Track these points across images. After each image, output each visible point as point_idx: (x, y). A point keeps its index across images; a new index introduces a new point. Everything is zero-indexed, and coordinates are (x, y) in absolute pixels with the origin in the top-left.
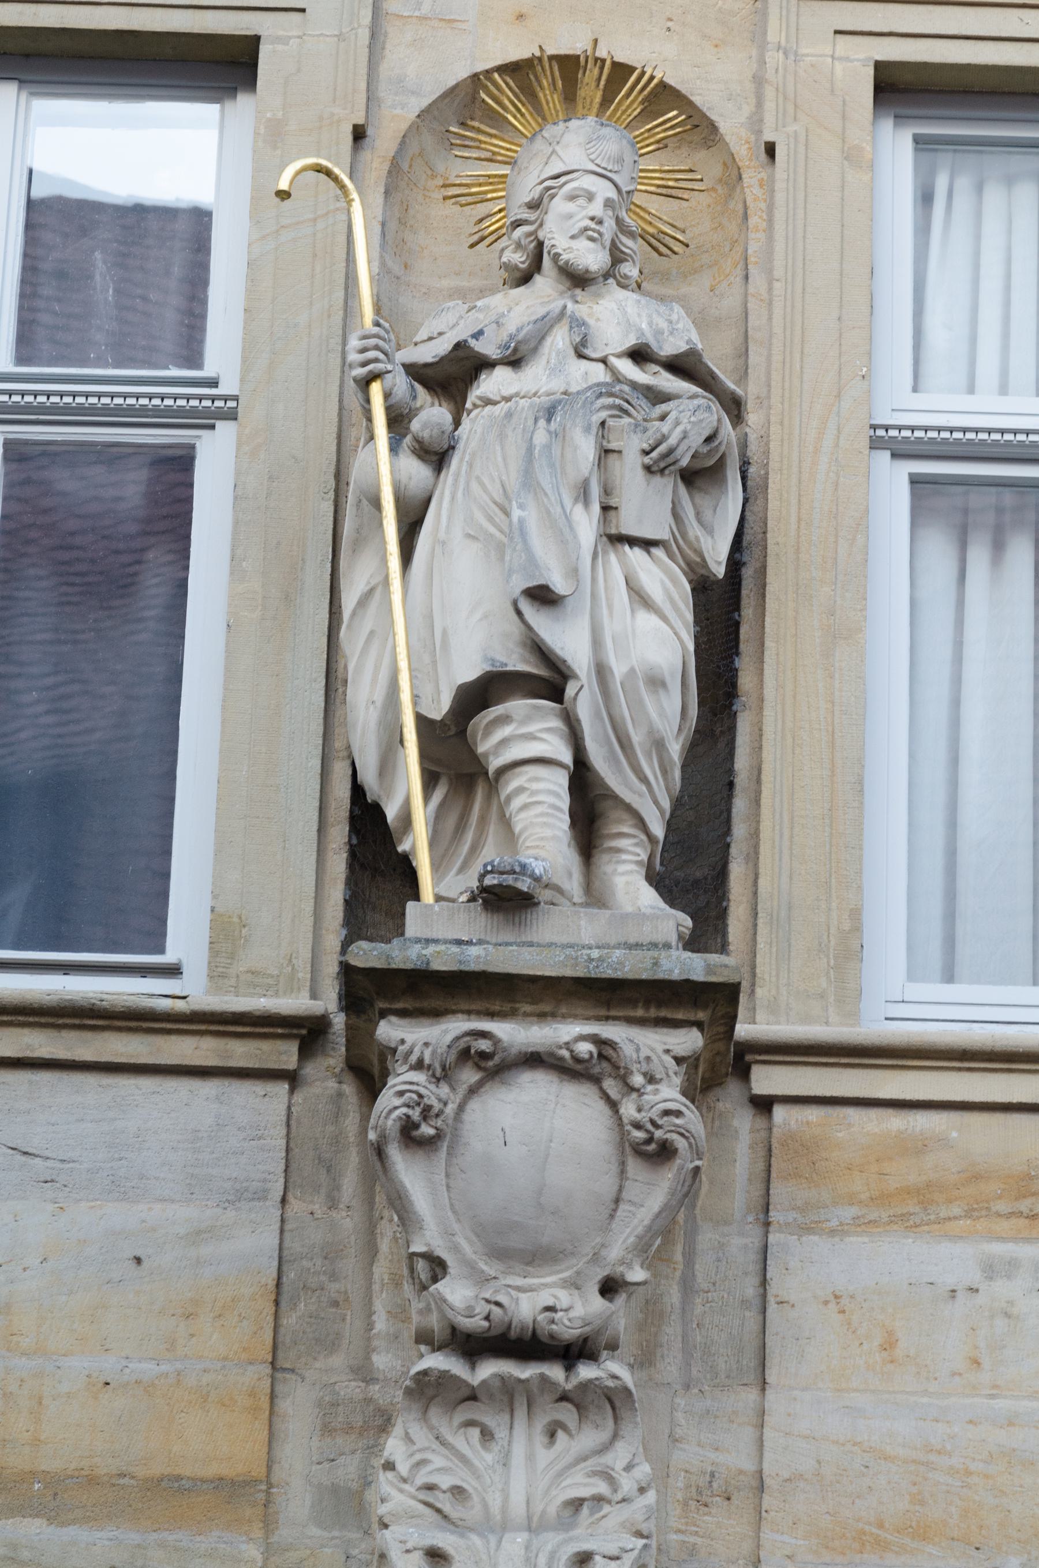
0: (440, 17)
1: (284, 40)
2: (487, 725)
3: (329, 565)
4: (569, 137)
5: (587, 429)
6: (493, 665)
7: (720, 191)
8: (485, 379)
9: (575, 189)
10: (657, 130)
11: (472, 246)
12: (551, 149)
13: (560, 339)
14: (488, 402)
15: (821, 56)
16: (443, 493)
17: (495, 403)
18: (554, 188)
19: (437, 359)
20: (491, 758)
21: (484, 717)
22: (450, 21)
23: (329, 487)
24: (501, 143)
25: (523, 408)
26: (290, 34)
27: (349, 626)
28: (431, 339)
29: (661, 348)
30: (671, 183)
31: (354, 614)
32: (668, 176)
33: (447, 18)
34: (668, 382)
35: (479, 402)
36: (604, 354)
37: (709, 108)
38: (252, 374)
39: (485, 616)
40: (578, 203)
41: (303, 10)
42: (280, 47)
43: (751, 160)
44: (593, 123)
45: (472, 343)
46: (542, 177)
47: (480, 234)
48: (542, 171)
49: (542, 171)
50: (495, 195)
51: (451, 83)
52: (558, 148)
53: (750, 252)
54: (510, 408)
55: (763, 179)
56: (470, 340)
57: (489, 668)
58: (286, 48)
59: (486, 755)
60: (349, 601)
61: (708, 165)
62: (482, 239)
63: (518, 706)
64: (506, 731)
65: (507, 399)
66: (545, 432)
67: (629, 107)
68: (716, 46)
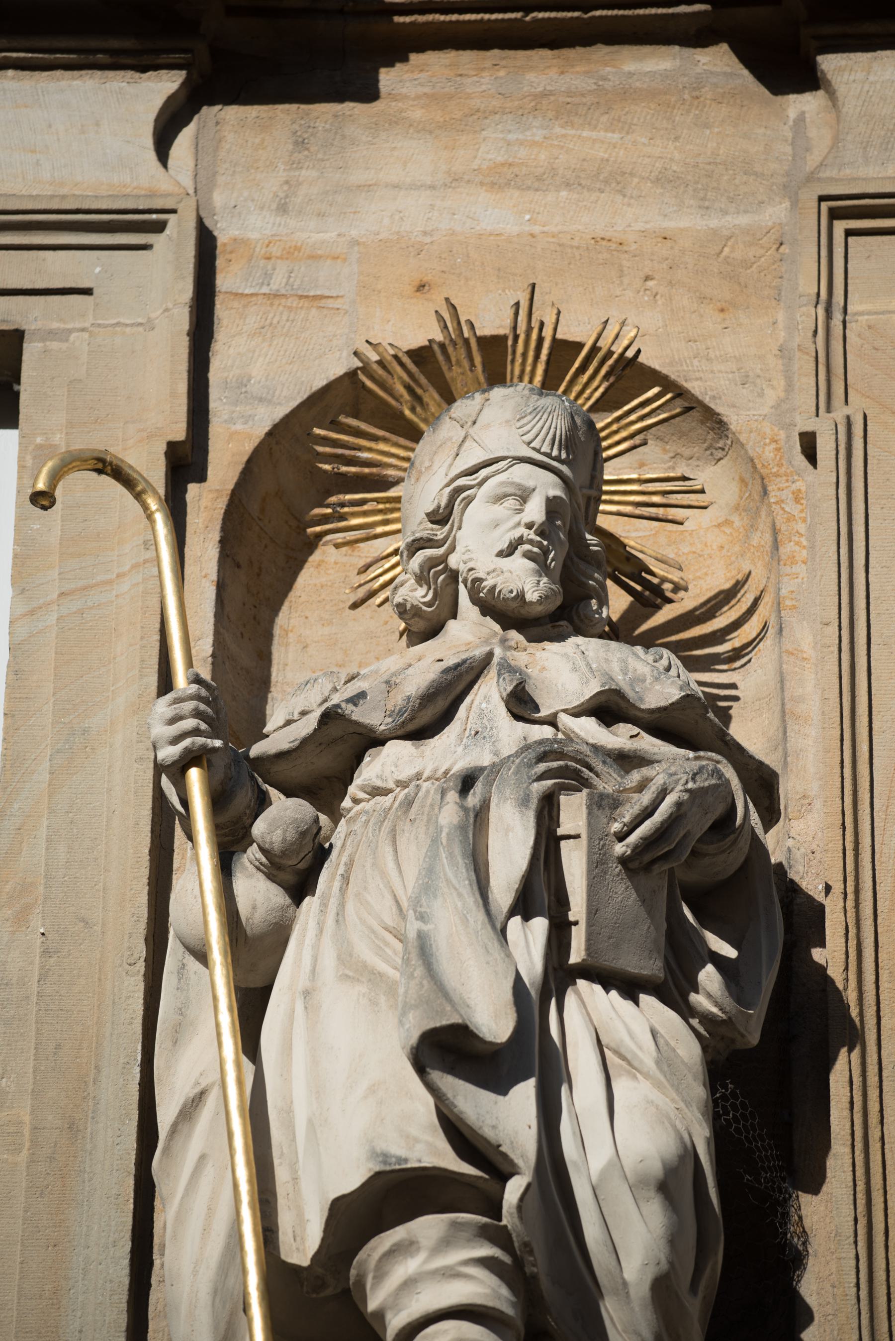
0: (300, 293)
1: (63, 335)
2: (380, 1260)
3: (137, 1070)
4: (488, 415)
5: (524, 802)
6: (385, 1163)
7: (737, 523)
8: (370, 762)
9: (502, 483)
10: (633, 417)
11: (355, 606)
12: (462, 433)
13: (488, 697)
14: (376, 792)
15: (883, 313)
16: (305, 930)
17: (385, 792)
18: (470, 487)
19: (297, 743)
20: (389, 1316)
21: (374, 1249)
22: (316, 298)
23: (136, 956)
24: (394, 450)
25: (428, 792)
26: (70, 326)
27: (166, 1149)
28: (288, 723)
29: (641, 699)
30: (656, 499)
31: (174, 1129)
32: (651, 487)
33: (312, 293)
34: (649, 744)
35: (362, 795)
36: (552, 711)
37: (713, 398)
38: (16, 806)
39: (372, 1090)
40: (504, 505)
41: (88, 292)
42: (54, 345)
43: (780, 465)
44: (526, 392)
45: (348, 709)
46: (452, 474)
47: (367, 587)
48: (451, 465)
49: (451, 465)
50: (388, 528)
51: (320, 382)
52: (472, 431)
53: (783, 592)
54: (406, 796)
55: (799, 490)
56: (343, 705)
57: (378, 1168)
58: (64, 346)
59: (380, 1315)
60: (165, 1117)
61: (716, 479)
62: (372, 594)
63: (428, 1227)
64: (410, 1266)
65: (402, 784)
66: (456, 807)
67: (586, 385)
68: (722, 310)
